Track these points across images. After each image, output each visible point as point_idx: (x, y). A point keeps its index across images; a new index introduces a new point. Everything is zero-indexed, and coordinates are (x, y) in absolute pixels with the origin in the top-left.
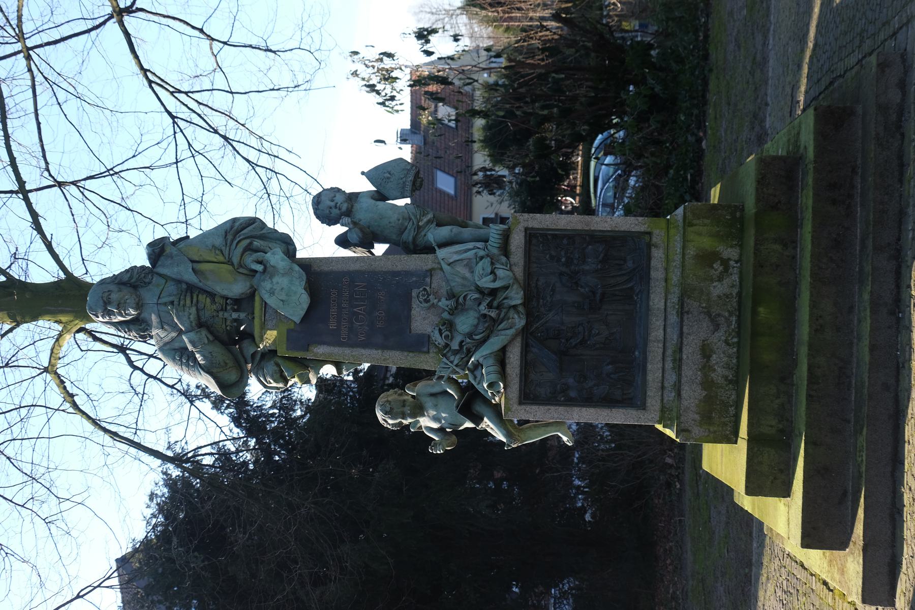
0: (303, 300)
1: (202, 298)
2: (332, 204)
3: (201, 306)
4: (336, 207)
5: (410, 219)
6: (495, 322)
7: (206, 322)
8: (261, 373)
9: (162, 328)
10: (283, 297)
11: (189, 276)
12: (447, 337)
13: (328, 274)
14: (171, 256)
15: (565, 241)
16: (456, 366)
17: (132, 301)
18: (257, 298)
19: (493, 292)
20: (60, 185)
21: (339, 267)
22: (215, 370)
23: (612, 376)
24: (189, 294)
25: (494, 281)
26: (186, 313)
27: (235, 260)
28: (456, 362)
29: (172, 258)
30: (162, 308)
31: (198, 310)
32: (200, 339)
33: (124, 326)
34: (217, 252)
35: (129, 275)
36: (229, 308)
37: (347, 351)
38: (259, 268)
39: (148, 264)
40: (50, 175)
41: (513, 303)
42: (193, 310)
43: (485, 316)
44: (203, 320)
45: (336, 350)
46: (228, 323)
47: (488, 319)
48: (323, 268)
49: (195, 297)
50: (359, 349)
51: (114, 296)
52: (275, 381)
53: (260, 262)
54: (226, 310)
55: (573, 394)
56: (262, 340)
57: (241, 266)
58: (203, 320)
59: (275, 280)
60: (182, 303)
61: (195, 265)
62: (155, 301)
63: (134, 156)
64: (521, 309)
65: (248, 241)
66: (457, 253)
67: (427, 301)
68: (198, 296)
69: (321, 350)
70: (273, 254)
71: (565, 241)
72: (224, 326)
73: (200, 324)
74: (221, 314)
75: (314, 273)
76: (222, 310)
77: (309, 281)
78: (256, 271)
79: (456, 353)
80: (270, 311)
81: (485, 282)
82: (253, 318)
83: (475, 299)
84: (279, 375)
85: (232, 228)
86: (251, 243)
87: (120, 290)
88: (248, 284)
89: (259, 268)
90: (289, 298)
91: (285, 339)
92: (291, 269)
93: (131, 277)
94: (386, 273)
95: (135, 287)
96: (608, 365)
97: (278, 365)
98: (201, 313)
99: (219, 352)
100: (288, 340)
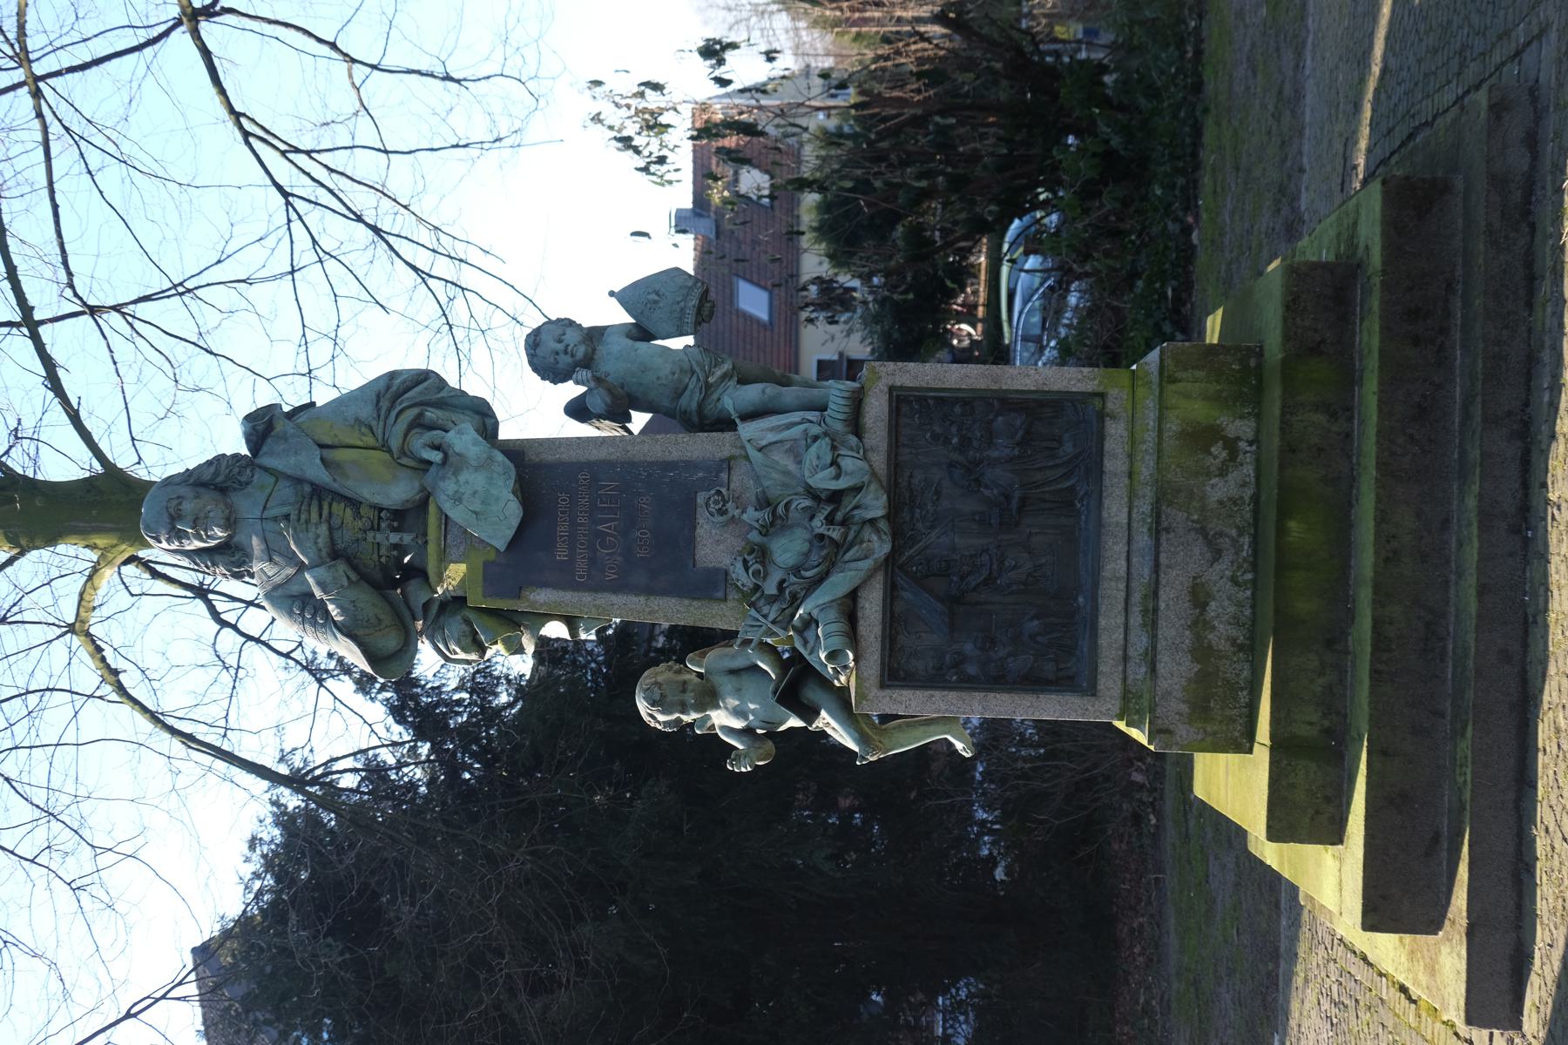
0: (513, 511)
1: (338, 508)
2: (560, 347)
3: (336, 522)
4: (566, 352)
5: (693, 372)
6: (839, 547)
10: (477, 507)
12: (756, 573)
14: (284, 437)
15: (958, 409)
16: (773, 622)
18: (432, 509)
19: (836, 497)
20: (93, 311)
22: (360, 632)
23: (1039, 639)
24: (315, 503)
25: (837, 477)
26: (311, 535)
27: (395, 443)
28: (772, 616)
29: (286, 440)
30: (269, 526)
31: (330, 529)
34: (363, 429)
35: (212, 469)
36: (383, 525)
37: (587, 598)
38: (436, 457)
39: (245, 451)
40: (76, 295)
41: (870, 515)
42: (323, 530)
43: (821, 537)
46: (383, 551)
47: (827, 542)
48: (544, 456)
51: (187, 506)
52: (464, 650)
53: (437, 448)
55: (972, 670)
56: (441, 580)
57: (405, 454)
58: (340, 546)
59: (462, 478)
60: (303, 517)
62: (258, 514)
63: (219, 262)
64: (883, 525)
65: (416, 411)
66: (772, 429)
67: (722, 512)
69: (541, 597)
70: (460, 432)
71: (958, 409)
72: (375, 557)
74: (370, 535)
75: (531, 466)
76: (372, 528)
77: (520, 480)
78: (430, 463)
79: (772, 600)
80: (453, 531)
81: (822, 479)
83: (805, 509)
84: (469, 639)
85: (388, 388)
86: (421, 415)
87: (197, 497)
88: (417, 484)
89: (436, 457)
90: (487, 509)
92: (490, 458)
93: (216, 474)
94: (651, 464)
95: (223, 490)
96: (1032, 619)
97: (468, 622)
98: (337, 535)
99: (366, 600)
100: (485, 579)
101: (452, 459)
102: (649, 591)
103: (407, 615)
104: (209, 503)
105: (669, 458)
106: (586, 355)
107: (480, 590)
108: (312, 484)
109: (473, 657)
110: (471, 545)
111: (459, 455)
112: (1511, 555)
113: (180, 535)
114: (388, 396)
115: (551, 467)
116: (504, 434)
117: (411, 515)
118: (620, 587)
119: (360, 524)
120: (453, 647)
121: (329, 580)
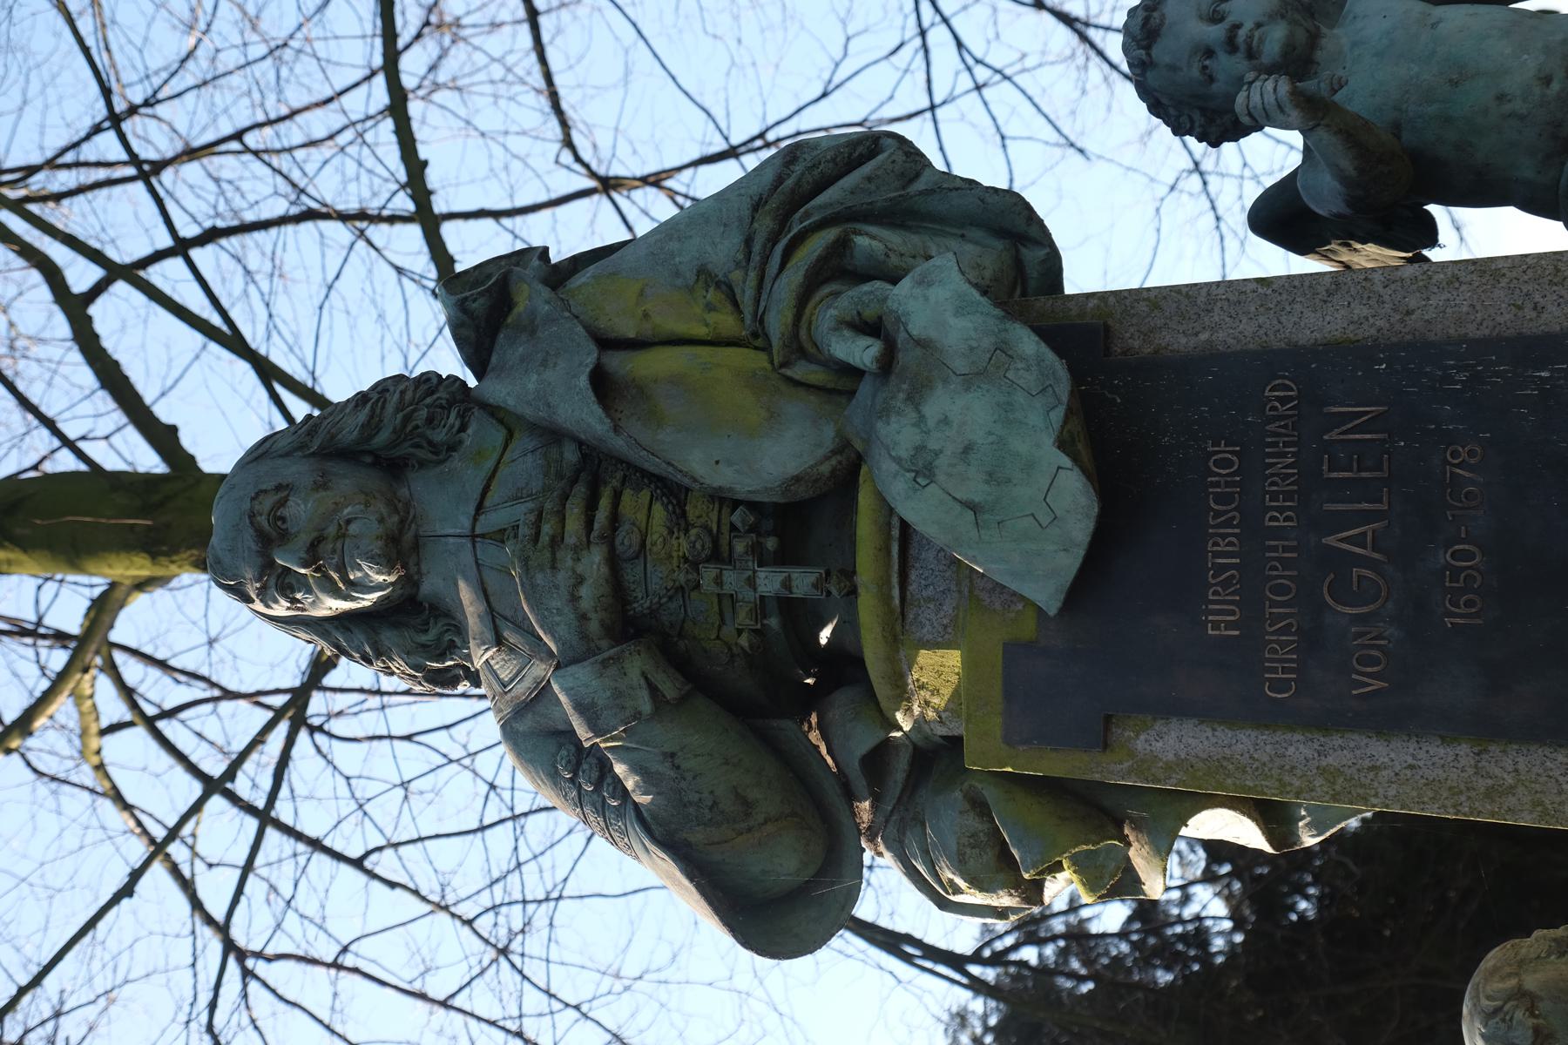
0: (1072, 501)
3: (627, 540)
4: (1231, 44)
8: (913, 847)
9: (499, 641)
10: (976, 490)
11: (580, 412)
14: (530, 328)
17: (367, 526)
18: (865, 499)
21: (1246, 327)
22: (697, 836)
24: (580, 490)
26: (562, 577)
27: (778, 323)
29: (533, 332)
30: (488, 552)
31: (614, 562)
32: (618, 694)
34: (712, 295)
35: (363, 416)
36: (740, 547)
37: (1299, 748)
38: (861, 352)
39: (448, 362)
40: (578, 159)
42: (595, 561)
44: (641, 605)
48: (1165, 339)
49: (604, 503)
50: (1356, 739)
51: (300, 510)
52: (978, 884)
53: (871, 327)
54: (730, 560)
56: (902, 695)
57: (802, 353)
58: (641, 604)
59: (938, 404)
60: (547, 529)
61: (619, 363)
62: (467, 523)
65: (830, 234)
68: (617, 497)
69: (1169, 744)
70: (924, 282)
74: (708, 573)
75: (1131, 376)
78: (856, 373)
84: (990, 856)
85: (779, 180)
87: (322, 485)
88: (829, 433)
89: (861, 352)
90: (990, 484)
92: (1003, 348)
93: (372, 426)
95: (392, 467)
98: (632, 574)
99: (710, 752)
100: (1008, 695)
101: (907, 357)
102: (1485, 729)
104: (354, 501)
105: (1533, 324)
106: (1289, 48)
107: (996, 724)
109: (1004, 900)
110: (979, 595)
111: (923, 344)
112: (81, 387)
113: (286, 585)
114: (773, 204)
116: (1079, 278)
117: (808, 519)
118: (1387, 718)
119: (683, 545)
120: (947, 874)
121: (602, 698)
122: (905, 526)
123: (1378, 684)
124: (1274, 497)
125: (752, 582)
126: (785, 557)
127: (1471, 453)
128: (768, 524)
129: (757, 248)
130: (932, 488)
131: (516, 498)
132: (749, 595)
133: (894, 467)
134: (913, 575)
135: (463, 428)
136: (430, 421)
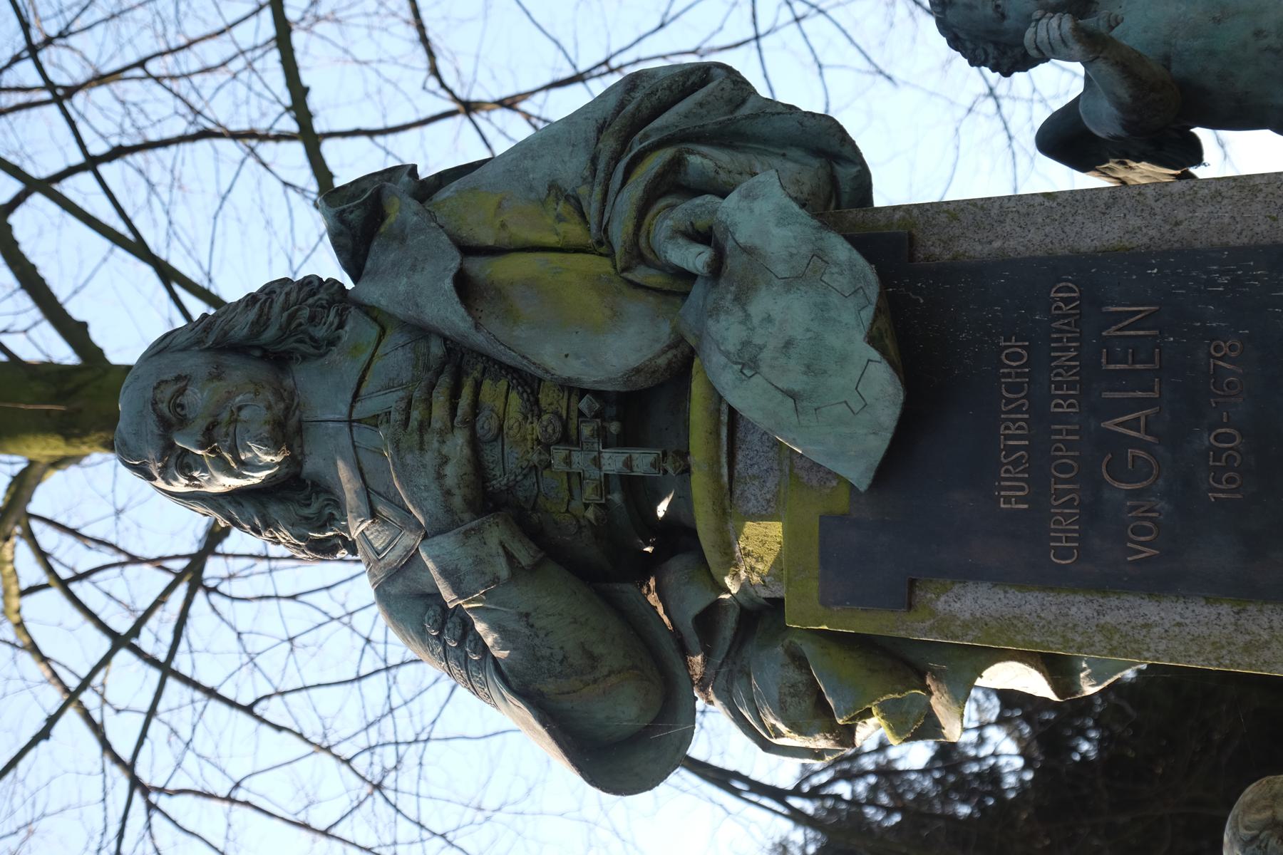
0: (879, 390)
1: (492, 392)
3: (486, 424)
7: (510, 489)
9: (373, 514)
10: (795, 380)
11: (446, 312)
13: (979, 271)
14: (400, 237)
20: (469, 108)
21: (1035, 236)
22: (549, 687)
24: (445, 381)
26: (430, 458)
27: (620, 232)
29: (403, 240)
31: (475, 443)
32: (478, 561)
33: (250, 510)
34: (562, 207)
35: (252, 314)
36: (586, 430)
37: (1080, 608)
38: (695, 258)
39: (328, 266)
40: (443, 85)
42: (458, 444)
44: (499, 482)
45: (1033, 605)
49: (467, 393)
50: (1130, 600)
51: (198, 398)
53: (702, 236)
54: (578, 443)
56: (730, 561)
58: (499, 482)
59: (761, 304)
60: (416, 415)
61: (481, 268)
62: (344, 409)
63: (662, 26)
65: (667, 154)
69: (965, 605)
70: (750, 196)
73: (486, 499)
74: (559, 454)
75: (928, 281)
78: (687, 277)
82: (687, 470)
85: (622, 105)
86: (677, 164)
87: (217, 376)
88: (665, 331)
89: (695, 258)
90: (809, 378)
91: (814, 558)
92: (819, 255)
93: (261, 323)
94: (1241, 254)
95: (278, 360)
98: (491, 455)
99: (561, 610)
100: (825, 561)
101: (734, 263)
102: (1243, 591)
103: (669, 649)
104: (245, 391)
108: (445, 339)
110: (799, 474)
111: (749, 251)
113: (185, 465)
114: (616, 126)
115: (976, 273)
117: (647, 406)
120: (770, 720)
121: (465, 564)
122: (733, 412)
123: (1149, 552)
124: (1059, 387)
125: (597, 462)
126: (628, 439)
127: (1232, 348)
128: (612, 411)
129: (601, 165)
130: (757, 379)
131: (388, 388)
132: (594, 473)
133: (723, 360)
134: (740, 456)
135: (341, 326)
136: (312, 319)
